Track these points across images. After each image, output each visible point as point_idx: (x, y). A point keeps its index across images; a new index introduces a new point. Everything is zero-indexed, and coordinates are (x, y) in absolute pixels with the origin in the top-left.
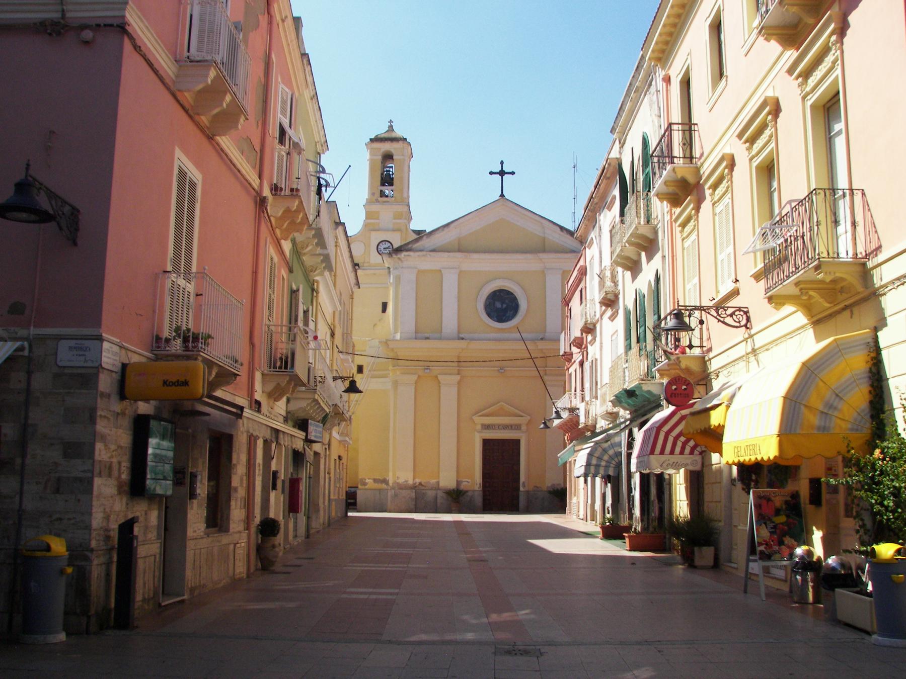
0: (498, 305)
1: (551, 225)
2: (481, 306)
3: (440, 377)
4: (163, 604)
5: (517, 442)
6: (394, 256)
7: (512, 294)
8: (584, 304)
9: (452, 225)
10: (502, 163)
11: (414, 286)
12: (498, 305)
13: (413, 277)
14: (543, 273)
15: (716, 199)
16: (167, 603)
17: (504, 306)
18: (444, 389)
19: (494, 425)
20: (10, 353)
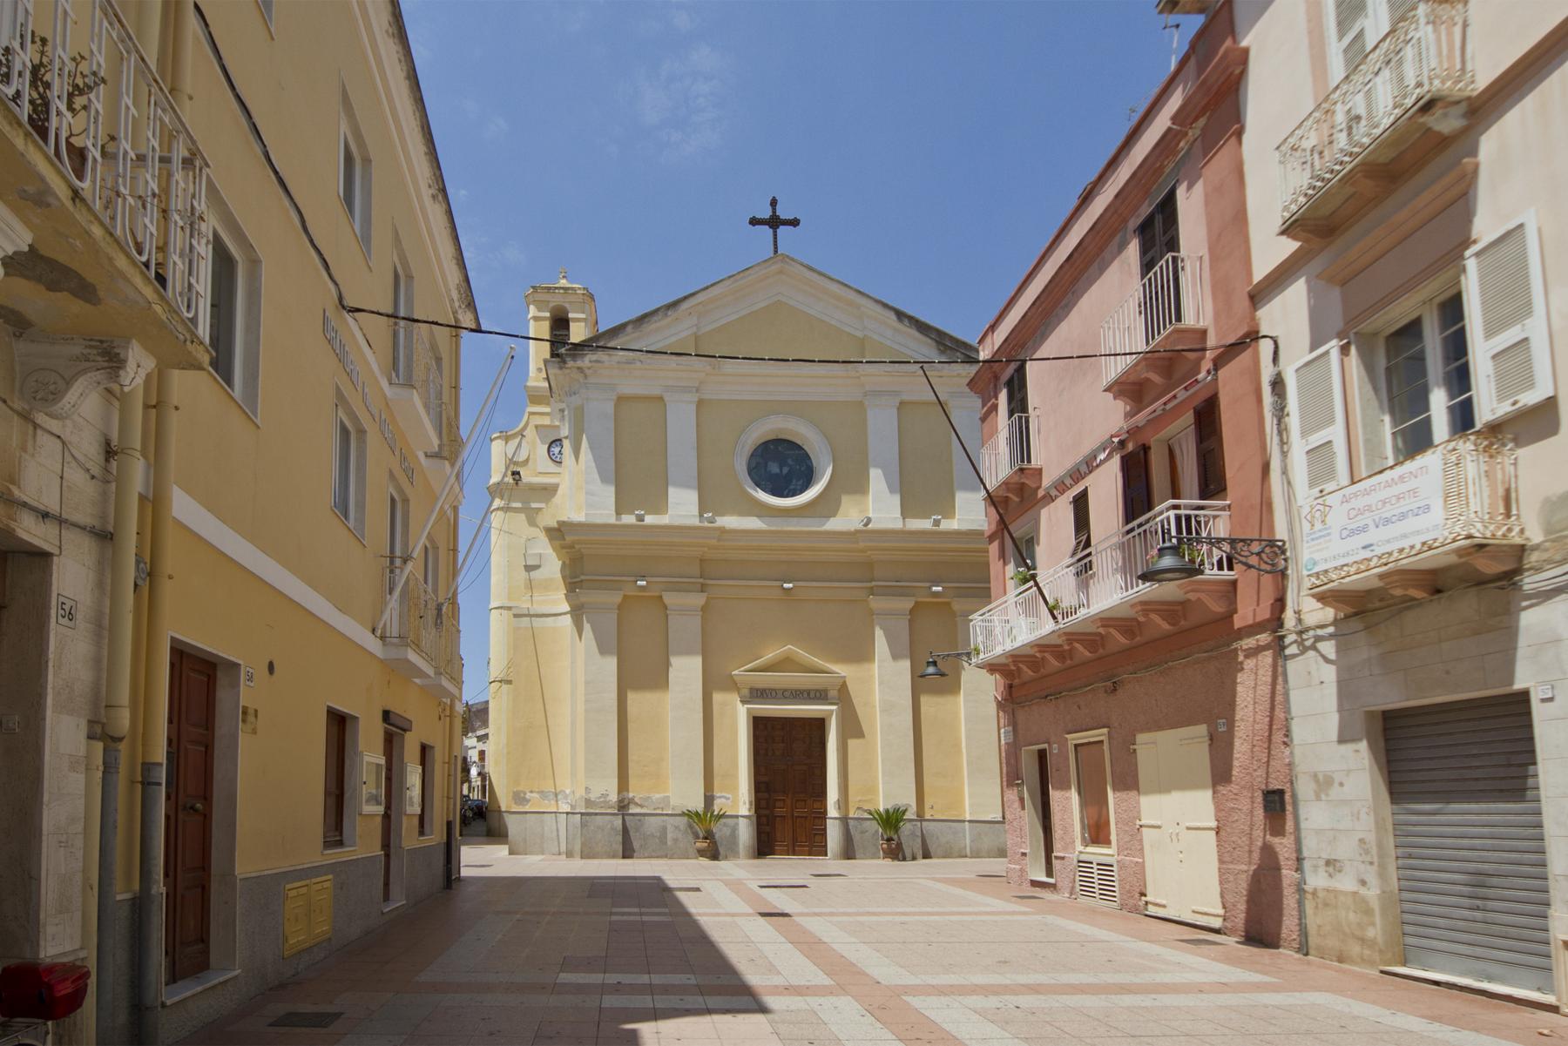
0: (774, 468)
1: (879, 309)
2: (741, 466)
3: (669, 598)
4: (169, 1003)
5: (819, 725)
6: (570, 363)
7: (800, 448)
8: (1501, 492)
9: (685, 306)
10: (774, 203)
11: (612, 425)
12: (774, 468)
13: (610, 408)
14: (860, 407)
15: (1119, 288)
16: (176, 999)
17: (785, 470)
18: (675, 622)
19: (771, 690)
20: (1467, 321)
